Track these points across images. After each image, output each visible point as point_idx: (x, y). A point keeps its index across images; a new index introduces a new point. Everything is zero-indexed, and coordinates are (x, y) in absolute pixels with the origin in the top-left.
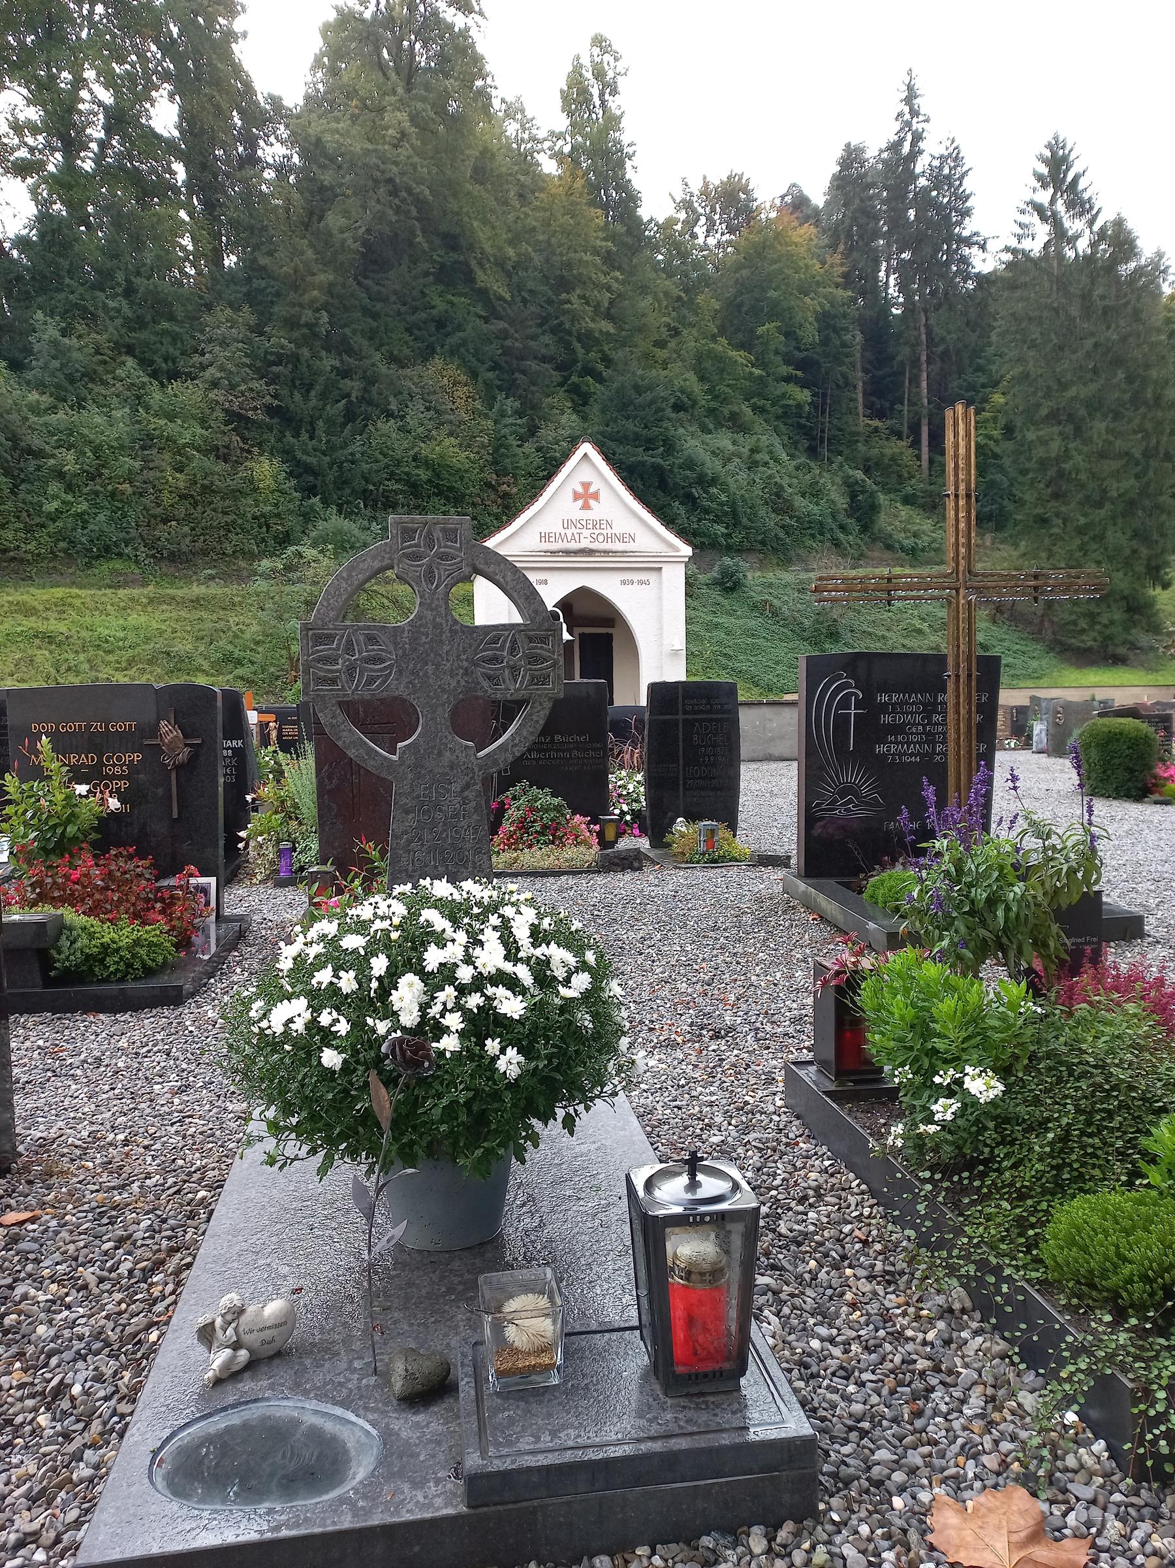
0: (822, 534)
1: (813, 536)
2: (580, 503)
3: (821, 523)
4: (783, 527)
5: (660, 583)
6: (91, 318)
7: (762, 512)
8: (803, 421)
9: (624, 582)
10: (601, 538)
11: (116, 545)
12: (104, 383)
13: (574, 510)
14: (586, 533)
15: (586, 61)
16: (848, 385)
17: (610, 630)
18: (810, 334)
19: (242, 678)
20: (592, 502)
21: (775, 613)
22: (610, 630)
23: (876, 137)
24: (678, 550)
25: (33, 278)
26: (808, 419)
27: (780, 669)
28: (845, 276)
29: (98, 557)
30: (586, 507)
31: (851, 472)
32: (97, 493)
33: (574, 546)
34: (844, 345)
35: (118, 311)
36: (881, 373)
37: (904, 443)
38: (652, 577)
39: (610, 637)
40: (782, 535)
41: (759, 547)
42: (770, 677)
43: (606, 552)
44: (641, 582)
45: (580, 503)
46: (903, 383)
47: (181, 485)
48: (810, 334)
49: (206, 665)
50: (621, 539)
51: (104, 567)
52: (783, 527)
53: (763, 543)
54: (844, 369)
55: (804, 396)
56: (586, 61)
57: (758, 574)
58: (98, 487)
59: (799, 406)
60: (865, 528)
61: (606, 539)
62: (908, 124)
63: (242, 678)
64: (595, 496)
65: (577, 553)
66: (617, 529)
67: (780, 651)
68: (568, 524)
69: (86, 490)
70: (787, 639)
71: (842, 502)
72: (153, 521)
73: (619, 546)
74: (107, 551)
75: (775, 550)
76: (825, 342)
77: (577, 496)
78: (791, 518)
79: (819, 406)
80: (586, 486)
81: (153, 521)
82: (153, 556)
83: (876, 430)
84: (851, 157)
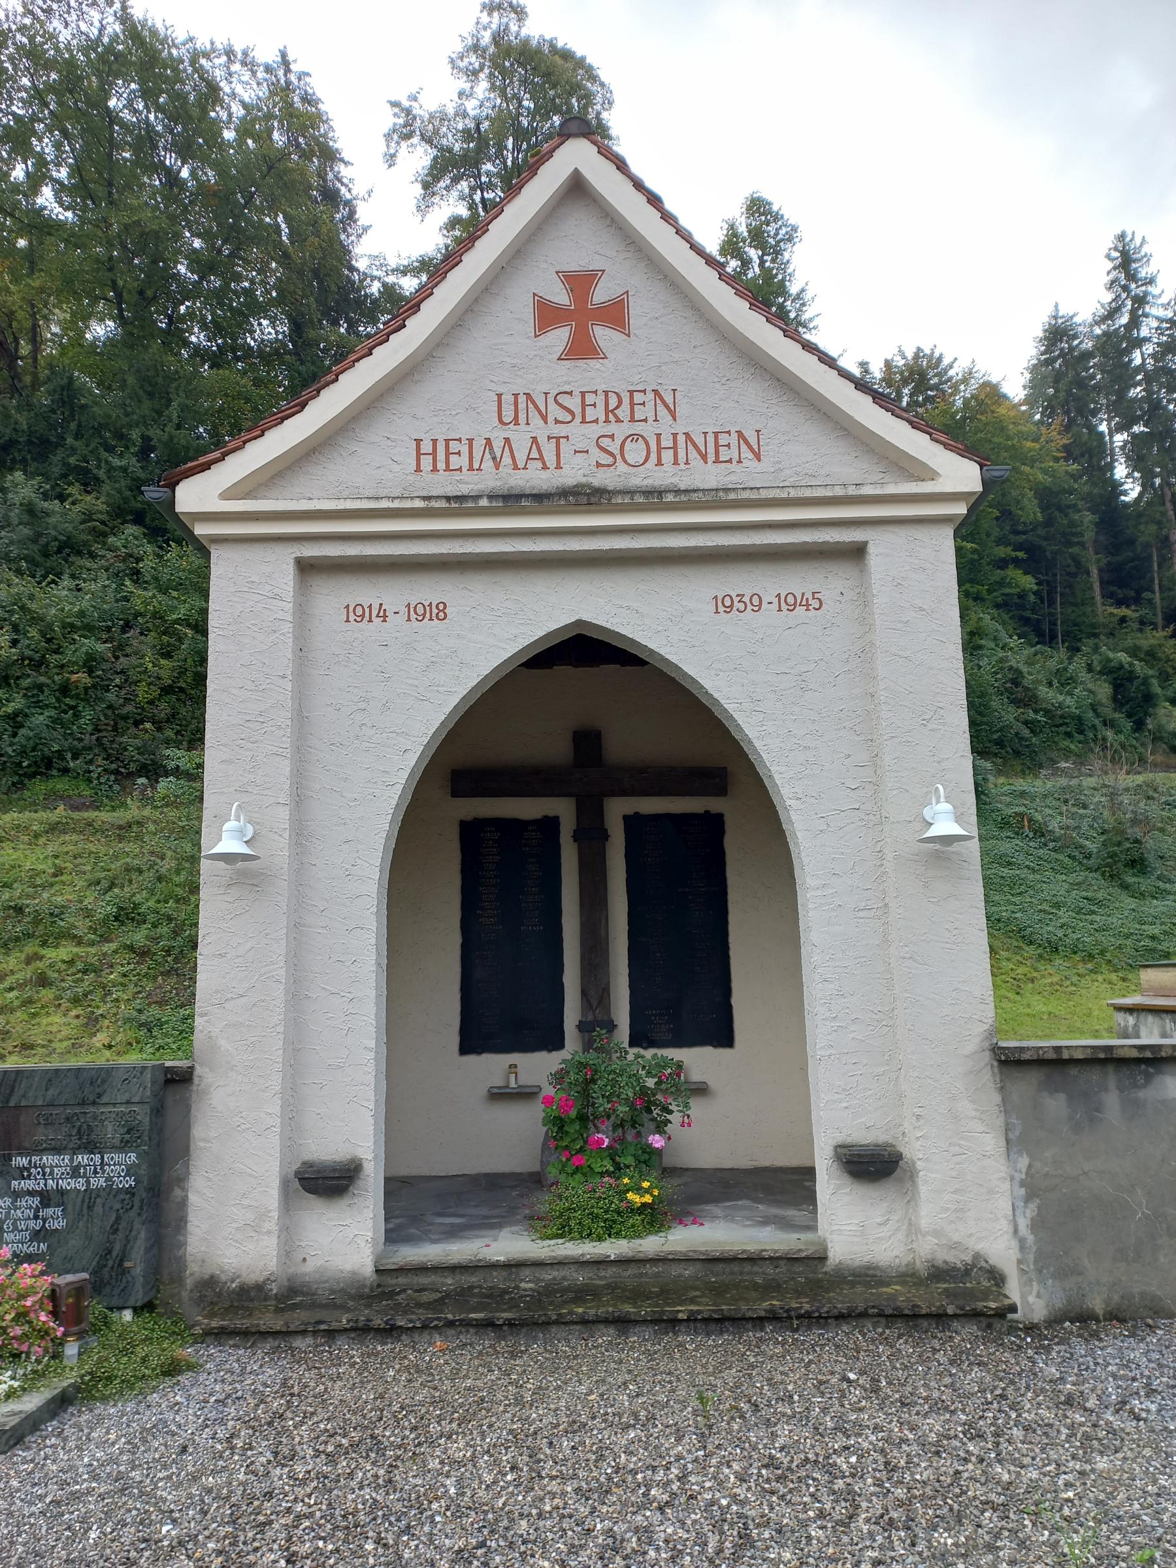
0: (1081, 732)
1: (1068, 735)
2: (560, 336)
3: (1079, 719)
4: (1026, 723)
5: (864, 599)
6: (89, 482)
7: (995, 703)
8: (1028, 614)
9: (725, 605)
10: (635, 452)
11: (60, 754)
12: (93, 556)
13: (541, 362)
14: (580, 434)
15: (743, 230)
16: (1080, 567)
17: (713, 804)
18: (1031, 510)
19: (131, 948)
20: (602, 335)
21: (1040, 832)
22: (713, 804)
23: (1086, 299)
24: (925, 472)
25: (30, 442)
26: (1033, 611)
27: (1064, 916)
28: (1066, 448)
29: (32, 776)
30: (582, 349)
31: (1111, 655)
32: (40, 687)
33: (536, 478)
34: (1072, 524)
35: (124, 469)
36: (1118, 558)
37: (1161, 634)
38: (829, 583)
39: (714, 825)
40: (1026, 732)
41: (995, 749)
42: (1051, 930)
43: (654, 498)
44: (787, 603)
45: (560, 336)
46: (1152, 566)
47: (164, 674)
48: (1031, 510)
49: (82, 926)
50: (711, 450)
51: (39, 787)
52: (1026, 723)
53: (1000, 743)
54: (1075, 550)
55: (1028, 582)
56: (743, 230)
57: (1002, 780)
58: (42, 679)
59: (1022, 596)
60: (1139, 726)
61: (655, 451)
62: (1125, 288)
63: (131, 948)
64: (615, 314)
65: (541, 500)
66: (695, 419)
67: (1058, 886)
68: (517, 407)
69: (26, 683)
70: (1067, 871)
71: (1104, 691)
72: (121, 724)
73: (705, 476)
74: (46, 765)
75: (1017, 753)
76: (1049, 522)
77: (547, 315)
78: (1036, 711)
79: (1047, 595)
80: (580, 283)
81: (121, 724)
82: (116, 772)
83: (1123, 620)
84: (1058, 334)
